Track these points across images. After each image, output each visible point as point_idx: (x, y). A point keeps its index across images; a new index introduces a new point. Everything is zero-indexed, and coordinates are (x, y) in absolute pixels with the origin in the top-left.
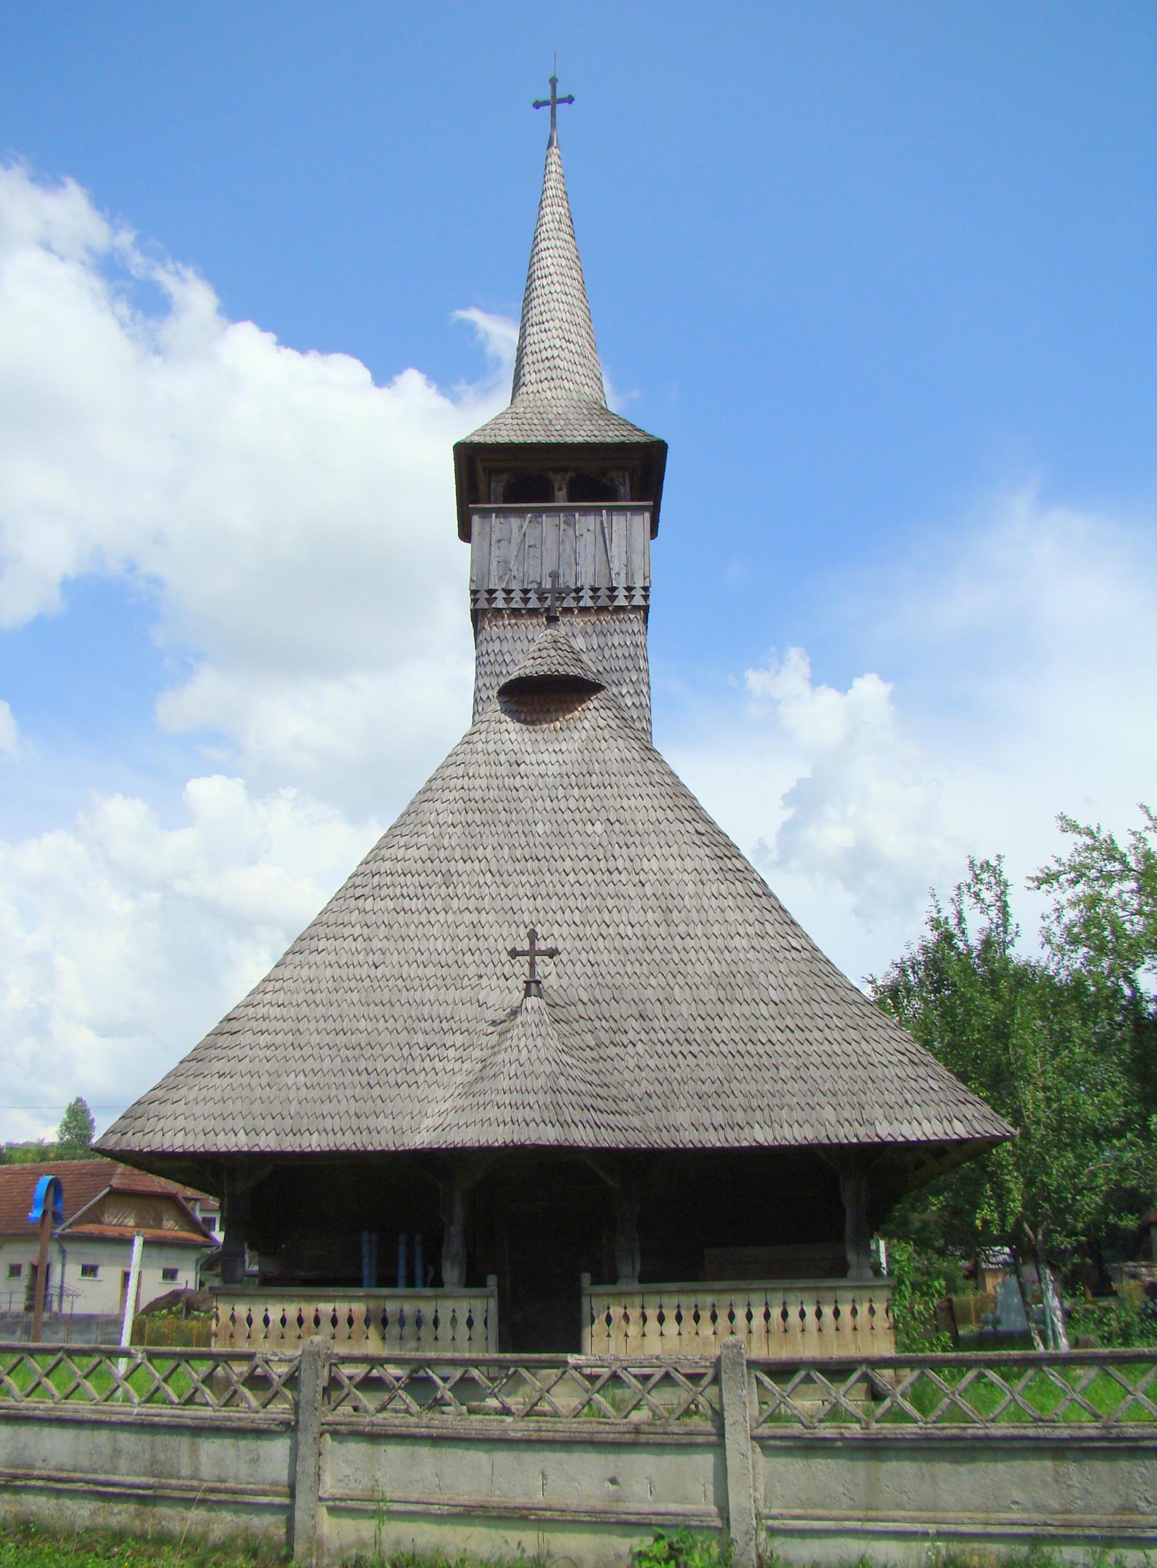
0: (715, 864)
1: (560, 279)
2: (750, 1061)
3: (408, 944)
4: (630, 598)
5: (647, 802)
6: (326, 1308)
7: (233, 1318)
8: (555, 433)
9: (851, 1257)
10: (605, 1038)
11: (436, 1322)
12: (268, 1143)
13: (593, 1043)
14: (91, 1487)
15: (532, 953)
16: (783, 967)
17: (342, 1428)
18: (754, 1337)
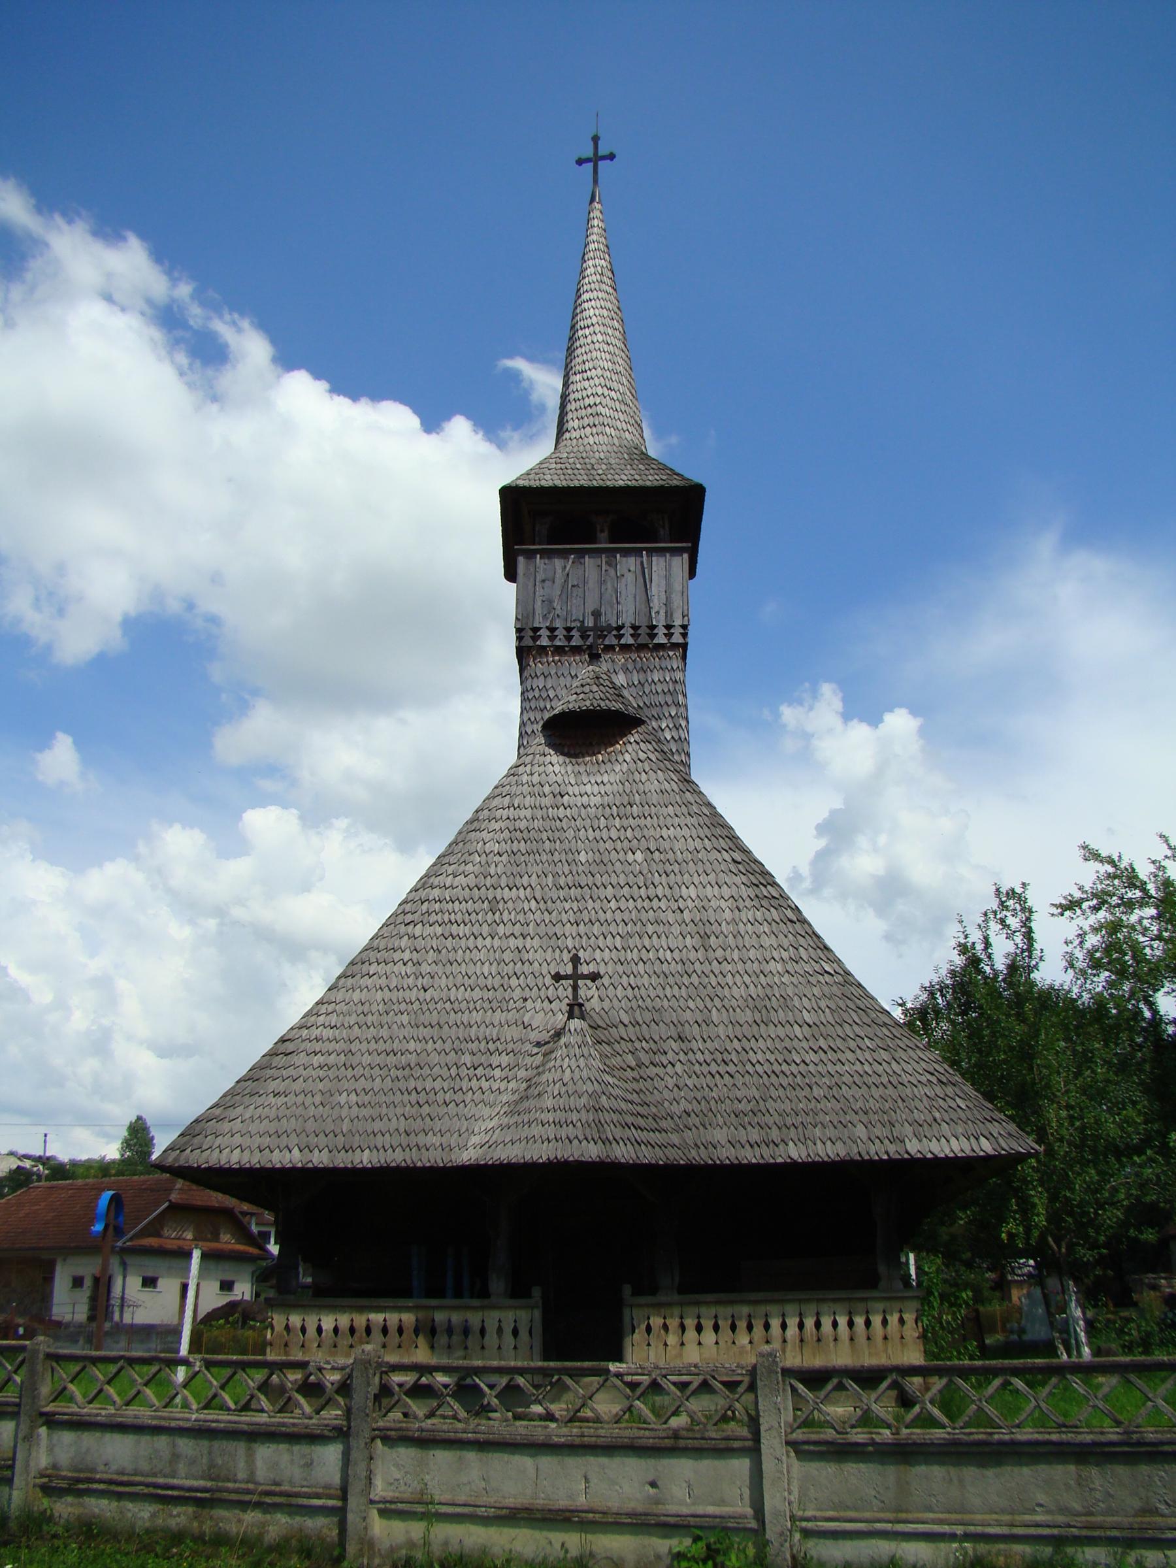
0: (751, 892)
1: (602, 329)
3: (455, 968)
4: (669, 635)
6: (377, 1318)
8: (597, 477)
10: (645, 1058)
11: (483, 1331)
12: (320, 1159)
13: (633, 1064)
14: (151, 1490)
16: (816, 991)
18: (789, 1346)
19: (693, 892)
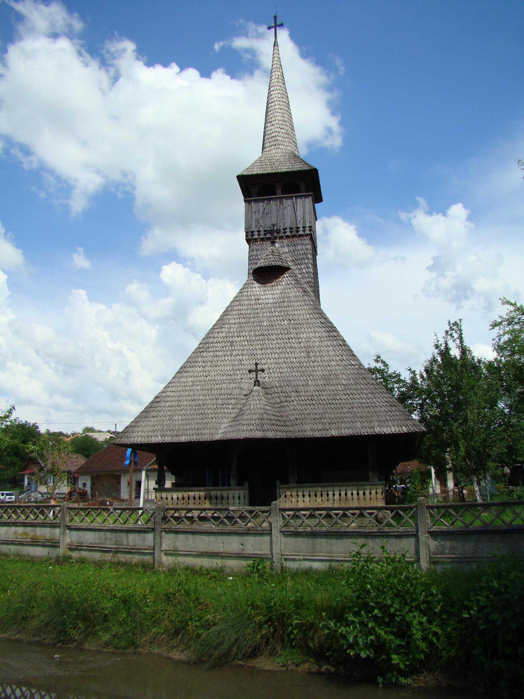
0: (327, 334)
1: (278, 103)
2: (333, 406)
3: (217, 368)
4: (304, 231)
5: (304, 312)
6: (192, 494)
7: (161, 498)
8: (275, 168)
9: (370, 474)
10: (283, 399)
11: (228, 498)
12: (168, 439)
13: (279, 401)
14: (99, 549)
15: (257, 371)
16: (348, 372)
17: (167, 530)
18: (336, 502)
19: (305, 335)
